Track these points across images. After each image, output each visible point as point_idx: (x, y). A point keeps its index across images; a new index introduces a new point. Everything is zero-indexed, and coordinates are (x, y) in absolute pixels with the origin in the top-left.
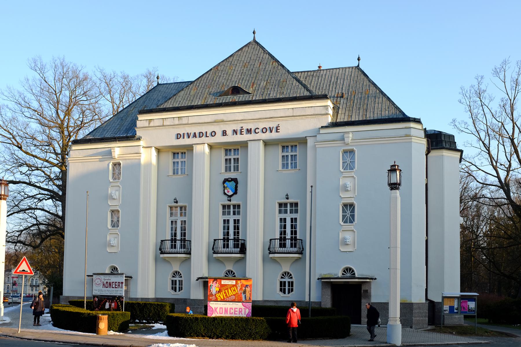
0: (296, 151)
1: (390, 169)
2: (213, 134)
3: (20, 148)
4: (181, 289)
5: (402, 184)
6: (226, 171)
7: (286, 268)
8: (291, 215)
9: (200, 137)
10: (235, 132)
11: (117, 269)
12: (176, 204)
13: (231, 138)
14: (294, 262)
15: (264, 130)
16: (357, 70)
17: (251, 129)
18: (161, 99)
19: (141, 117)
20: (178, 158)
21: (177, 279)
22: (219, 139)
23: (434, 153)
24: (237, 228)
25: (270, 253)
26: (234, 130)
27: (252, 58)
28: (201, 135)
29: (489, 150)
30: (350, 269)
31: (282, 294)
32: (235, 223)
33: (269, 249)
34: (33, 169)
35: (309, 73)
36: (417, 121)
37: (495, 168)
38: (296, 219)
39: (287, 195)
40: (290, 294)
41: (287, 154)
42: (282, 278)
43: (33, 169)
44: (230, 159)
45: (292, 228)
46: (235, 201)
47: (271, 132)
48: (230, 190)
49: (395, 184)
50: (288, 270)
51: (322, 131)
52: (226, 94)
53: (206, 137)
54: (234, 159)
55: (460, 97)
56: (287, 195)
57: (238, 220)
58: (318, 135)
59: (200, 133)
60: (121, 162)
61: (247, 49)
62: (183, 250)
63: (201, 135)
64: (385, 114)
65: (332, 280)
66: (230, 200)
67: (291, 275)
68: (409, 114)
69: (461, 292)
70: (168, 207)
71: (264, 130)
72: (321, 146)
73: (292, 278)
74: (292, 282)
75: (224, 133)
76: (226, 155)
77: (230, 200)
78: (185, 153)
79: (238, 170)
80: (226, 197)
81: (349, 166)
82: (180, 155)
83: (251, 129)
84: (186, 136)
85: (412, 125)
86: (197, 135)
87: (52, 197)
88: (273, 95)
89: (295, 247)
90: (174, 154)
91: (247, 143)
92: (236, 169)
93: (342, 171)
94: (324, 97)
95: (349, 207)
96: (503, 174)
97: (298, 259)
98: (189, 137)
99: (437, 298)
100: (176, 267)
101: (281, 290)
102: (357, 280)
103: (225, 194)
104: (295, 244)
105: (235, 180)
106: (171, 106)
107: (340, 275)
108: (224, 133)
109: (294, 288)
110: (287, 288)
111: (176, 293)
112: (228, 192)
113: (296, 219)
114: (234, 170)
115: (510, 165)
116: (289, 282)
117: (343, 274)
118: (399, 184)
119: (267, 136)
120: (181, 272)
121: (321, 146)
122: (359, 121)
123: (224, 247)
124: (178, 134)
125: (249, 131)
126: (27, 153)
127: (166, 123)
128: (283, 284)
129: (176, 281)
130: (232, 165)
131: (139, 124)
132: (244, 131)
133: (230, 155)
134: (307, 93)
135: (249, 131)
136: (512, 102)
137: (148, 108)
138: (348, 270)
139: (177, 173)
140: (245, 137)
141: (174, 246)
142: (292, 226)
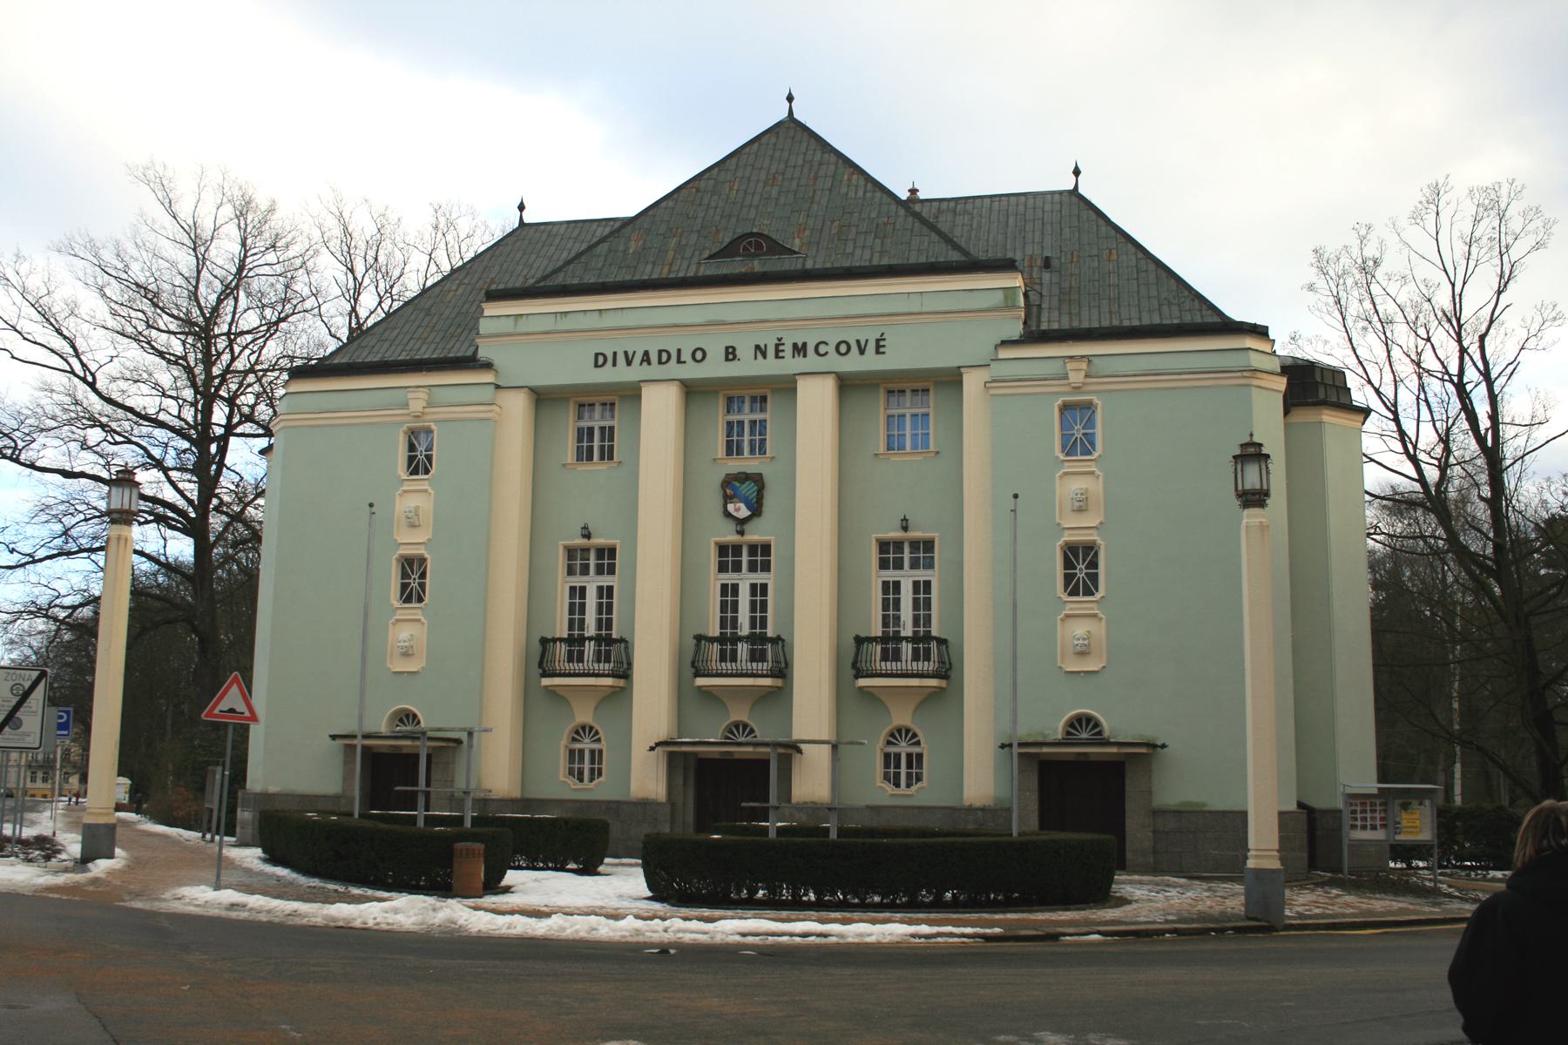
0: (763, 410)
1: (1238, 452)
2: (699, 355)
3: (92, 385)
4: (596, 773)
5: (1272, 492)
6: (729, 452)
7: (584, 715)
8: (600, 578)
9: (660, 362)
10: (760, 351)
11: (415, 716)
12: (583, 542)
13: (748, 366)
14: (925, 701)
15: (843, 349)
16: (1074, 199)
17: (805, 344)
18: (548, 263)
19: (491, 309)
20: (591, 418)
21: (587, 745)
22: (716, 368)
23: (1302, 416)
24: (605, 608)
25: (857, 677)
26: (757, 347)
27: (792, 163)
28: (664, 357)
29: (1395, 413)
30: (1089, 719)
31: (889, 788)
32: (601, 597)
33: (854, 665)
34: (119, 439)
35: (944, 205)
36: (1260, 332)
37: (1414, 459)
38: (610, 589)
39: (905, 520)
40: (914, 788)
41: (739, 417)
42: (889, 743)
43: (119, 439)
44: (591, 430)
45: (600, 612)
46: (754, 535)
47: (862, 352)
48: (742, 506)
49: (1254, 492)
50: (745, 719)
51: (1004, 353)
52: (728, 251)
53: (679, 361)
54: (602, 429)
55: (1312, 275)
56: (905, 520)
57: (764, 587)
58: (993, 365)
59: (660, 352)
60: (433, 426)
61: (773, 140)
62: (605, 667)
63: (664, 357)
64: (1172, 317)
65: (1045, 750)
66: (741, 533)
67: (915, 735)
68: (1236, 313)
69: (1382, 778)
70: (561, 550)
71: (843, 348)
72: (1209, 383)
73: (918, 743)
74: (920, 756)
75: (730, 354)
76: (580, 417)
77: (741, 533)
78: (613, 404)
79: (611, 458)
80: (732, 526)
81: (1080, 445)
82: (598, 408)
83: (805, 344)
84: (621, 359)
85: (1250, 342)
86: (654, 357)
87: (160, 519)
88: (861, 259)
89: (608, 660)
90: (581, 406)
91: (640, 389)
92: (759, 448)
93: (1062, 457)
94: (1007, 266)
95: (412, 566)
96: (1432, 474)
97: (937, 694)
98: (629, 363)
99: (1319, 803)
100: (584, 714)
101: (571, 772)
102: (1114, 750)
103: (727, 515)
104: (608, 653)
105: (758, 480)
106: (575, 281)
107: (383, 728)
108: (730, 354)
109: (925, 771)
110: (903, 770)
111: (580, 786)
112: (737, 510)
113: (928, 584)
114: (602, 458)
115: (1447, 451)
116: (909, 756)
117: (1068, 733)
118: (1267, 494)
119: (853, 364)
120: (597, 727)
121: (1209, 383)
122: (1172, 325)
123: (570, 660)
124: (597, 355)
125: (800, 350)
126: (110, 401)
127: (523, 326)
128: (890, 760)
129: (898, 756)
130: (596, 444)
131: (485, 326)
132: (788, 348)
133: (591, 418)
134: (955, 256)
135: (800, 350)
136: (1458, 290)
137: (501, 286)
138: (407, 717)
139: (902, 447)
140: (791, 364)
141: (729, 656)
142: (600, 605)
